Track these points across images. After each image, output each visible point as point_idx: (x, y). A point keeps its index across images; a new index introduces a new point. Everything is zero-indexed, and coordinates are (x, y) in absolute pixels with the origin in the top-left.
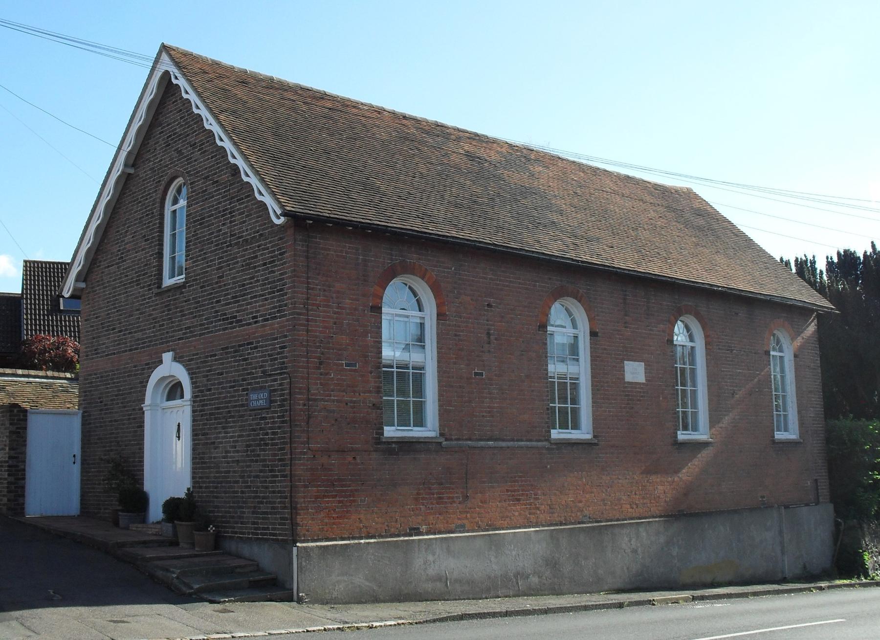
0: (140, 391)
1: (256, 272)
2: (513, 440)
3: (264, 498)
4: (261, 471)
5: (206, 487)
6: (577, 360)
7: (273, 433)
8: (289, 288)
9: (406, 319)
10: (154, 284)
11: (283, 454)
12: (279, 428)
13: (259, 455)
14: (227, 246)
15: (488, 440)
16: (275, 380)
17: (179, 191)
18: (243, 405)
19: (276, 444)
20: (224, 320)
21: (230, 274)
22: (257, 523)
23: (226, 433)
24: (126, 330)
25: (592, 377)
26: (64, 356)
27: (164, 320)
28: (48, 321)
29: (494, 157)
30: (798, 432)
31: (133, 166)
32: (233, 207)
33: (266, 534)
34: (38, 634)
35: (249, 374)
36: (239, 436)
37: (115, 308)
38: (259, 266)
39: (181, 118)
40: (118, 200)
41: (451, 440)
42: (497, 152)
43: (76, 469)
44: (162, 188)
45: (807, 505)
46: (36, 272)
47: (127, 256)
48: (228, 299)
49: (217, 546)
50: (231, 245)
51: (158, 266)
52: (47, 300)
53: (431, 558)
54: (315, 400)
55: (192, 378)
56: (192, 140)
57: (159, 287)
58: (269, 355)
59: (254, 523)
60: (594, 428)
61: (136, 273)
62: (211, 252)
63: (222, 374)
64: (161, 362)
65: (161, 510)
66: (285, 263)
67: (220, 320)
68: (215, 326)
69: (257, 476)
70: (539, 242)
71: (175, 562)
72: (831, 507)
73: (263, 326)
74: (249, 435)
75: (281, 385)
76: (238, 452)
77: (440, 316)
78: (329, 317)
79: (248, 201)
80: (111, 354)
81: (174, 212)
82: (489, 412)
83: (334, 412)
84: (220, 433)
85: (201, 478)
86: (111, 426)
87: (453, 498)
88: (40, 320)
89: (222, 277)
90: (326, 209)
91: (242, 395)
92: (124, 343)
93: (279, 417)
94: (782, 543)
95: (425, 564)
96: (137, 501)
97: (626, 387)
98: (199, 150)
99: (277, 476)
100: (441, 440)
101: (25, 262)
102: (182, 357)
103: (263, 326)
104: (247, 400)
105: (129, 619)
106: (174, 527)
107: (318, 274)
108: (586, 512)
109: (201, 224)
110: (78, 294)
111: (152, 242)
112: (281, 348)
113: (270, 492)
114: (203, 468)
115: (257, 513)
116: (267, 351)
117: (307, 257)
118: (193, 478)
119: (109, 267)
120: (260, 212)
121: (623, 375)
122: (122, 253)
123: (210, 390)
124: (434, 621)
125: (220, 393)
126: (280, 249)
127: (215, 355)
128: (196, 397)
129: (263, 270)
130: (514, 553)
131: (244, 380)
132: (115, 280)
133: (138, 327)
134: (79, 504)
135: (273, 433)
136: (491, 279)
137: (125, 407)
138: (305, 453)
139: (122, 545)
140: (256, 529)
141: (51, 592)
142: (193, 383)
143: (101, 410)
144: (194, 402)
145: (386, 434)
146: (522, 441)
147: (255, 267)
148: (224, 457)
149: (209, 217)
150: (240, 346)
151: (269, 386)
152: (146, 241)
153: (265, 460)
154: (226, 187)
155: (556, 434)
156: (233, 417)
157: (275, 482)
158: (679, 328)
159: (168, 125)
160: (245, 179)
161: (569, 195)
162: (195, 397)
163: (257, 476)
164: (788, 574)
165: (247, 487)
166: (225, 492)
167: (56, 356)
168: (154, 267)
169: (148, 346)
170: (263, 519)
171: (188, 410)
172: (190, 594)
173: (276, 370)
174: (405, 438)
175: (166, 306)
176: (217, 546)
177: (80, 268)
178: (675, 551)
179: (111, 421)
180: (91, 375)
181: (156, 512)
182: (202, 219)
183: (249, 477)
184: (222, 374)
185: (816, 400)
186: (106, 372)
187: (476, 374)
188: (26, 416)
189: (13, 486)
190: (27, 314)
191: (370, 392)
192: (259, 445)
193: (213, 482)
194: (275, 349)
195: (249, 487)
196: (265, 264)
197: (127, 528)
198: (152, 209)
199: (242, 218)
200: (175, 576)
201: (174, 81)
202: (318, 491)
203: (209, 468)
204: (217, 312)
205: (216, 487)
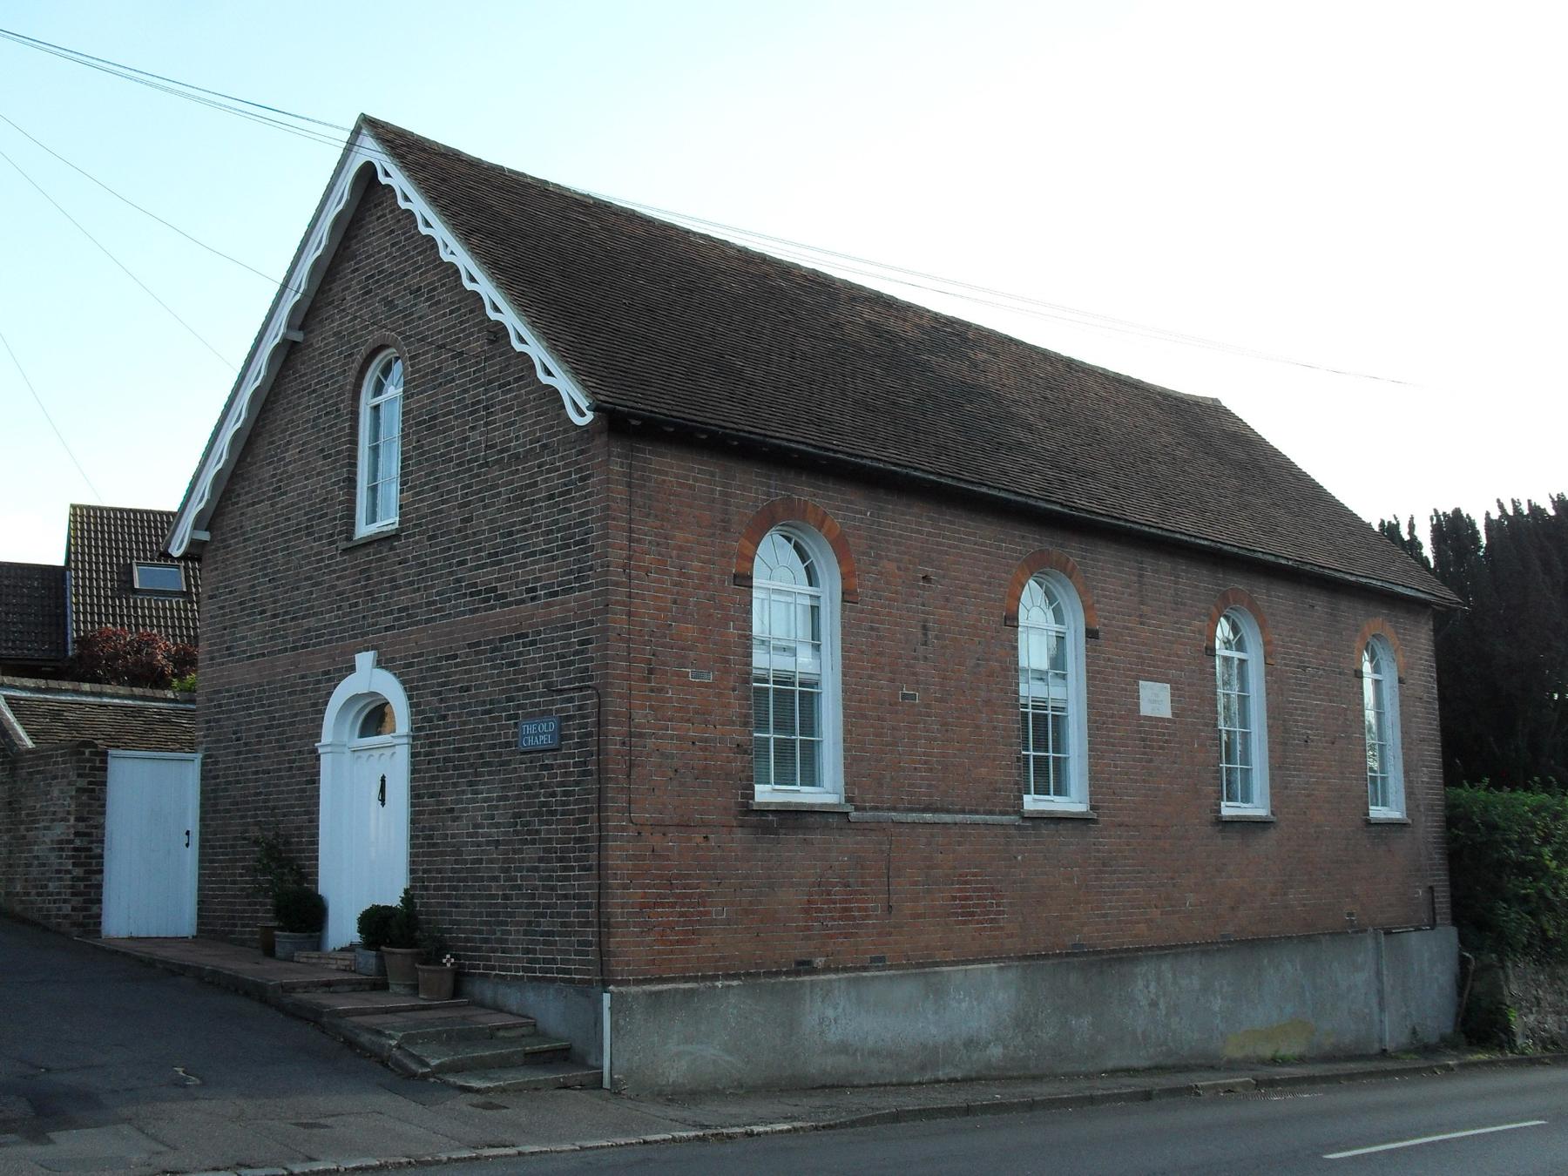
0: (313, 720)
1: (534, 511)
2: (963, 812)
3: (547, 906)
4: (541, 860)
5: (437, 888)
6: (1064, 677)
7: (565, 794)
8: (598, 538)
9: (789, 599)
10: (341, 533)
11: (584, 830)
12: (577, 783)
13: (538, 832)
14: (481, 466)
15: (925, 810)
16: (571, 700)
17: (386, 371)
18: (508, 744)
19: (572, 812)
20: (472, 594)
21: (484, 516)
22: (534, 951)
23: (476, 792)
24: (286, 613)
25: (1089, 706)
26: (150, 664)
27: (357, 596)
28: (114, 608)
29: (912, 333)
30: (1404, 807)
31: (301, 328)
32: (492, 398)
33: (550, 971)
34: (176, 1149)
35: (519, 689)
36: (500, 799)
37: (266, 575)
38: (540, 500)
39: (393, 245)
40: (272, 388)
41: (864, 809)
42: (917, 326)
43: (191, 856)
44: (356, 366)
45: (1418, 929)
46: (92, 526)
47: (288, 485)
48: (480, 558)
49: (457, 992)
50: (486, 464)
51: (348, 501)
52: (112, 572)
53: (830, 1013)
54: (641, 735)
55: (410, 698)
56: (413, 281)
57: (349, 539)
58: (559, 656)
59: (527, 951)
60: (1091, 793)
61: (306, 514)
62: (449, 476)
63: (468, 689)
64: (352, 669)
65: (355, 926)
66: (590, 494)
67: (465, 595)
68: (455, 607)
69: (536, 869)
70: (1006, 474)
71: (389, 1018)
72: (1453, 931)
73: (548, 605)
74: (518, 797)
75: (580, 708)
76: (497, 825)
77: (848, 596)
78: (665, 591)
79: (520, 388)
80: (258, 656)
81: (376, 408)
82: (926, 763)
83: (672, 756)
84: (463, 792)
85: (425, 871)
86: (256, 780)
87: (866, 909)
88: (99, 606)
89: (469, 519)
90: (662, 405)
91: (508, 727)
92: (283, 637)
93: (575, 765)
94: (1380, 992)
95: (821, 1024)
96: (307, 913)
97: (1142, 725)
98: (427, 300)
99: (572, 869)
100: (849, 808)
101: (74, 507)
102: (393, 660)
103: (548, 605)
104: (515, 735)
105: (329, 1121)
106: (380, 958)
107: (648, 515)
109: (429, 428)
110: (194, 551)
111: (336, 461)
112: (582, 643)
113: (559, 897)
114: (430, 854)
115: (535, 933)
116: (554, 648)
117: (629, 485)
118: (412, 871)
119: (253, 504)
120: (542, 405)
121: (1138, 705)
122: (280, 481)
123: (444, 717)
124: (853, 1124)
125: (465, 723)
126: (581, 470)
127: (456, 657)
128: (419, 729)
129: (548, 507)
130: (964, 1005)
131: (509, 700)
132: (266, 527)
133: (308, 609)
134: (195, 921)
135: (565, 794)
136: (929, 534)
137: (283, 748)
138: (623, 829)
139: (290, 988)
140: (530, 961)
141: (180, 1070)
142: (411, 706)
143: (238, 753)
144: (414, 738)
145: (759, 798)
146: (977, 812)
147: (532, 502)
148: (469, 835)
149: (445, 415)
150: (502, 640)
151: (557, 711)
152: (325, 458)
153: (550, 841)
154: (477, 363)
155: (1031, 803)
156: (489, 764)
157: (567, 878)
158: (1223, 630)
159: (368, 258)
160: (518, 347)
161: (1035, 401)
162: (416, 731)
163: (536, 869)
164: (1390, 1046)
165: (513, 888)
166: (473, 897)
167: (135, 664)
168: (340, 503)
169: (326, 642)
170: (545, 943)
171: (403, 755)
172: (425, 1076)
173: (570, 681)
174: (788, 804)
175: (361, 572)
176: (457, 992)
177: (202, 506)
179: (257, 773)
180: (219, 692)
181: (343, 929)
182: (431, 419)
183: (519, 869)
184: (468, 689)
185: (1432, 753)
186: (248, 687)
187: (904, 696)
188: (105, 762)
189: (82, 884)
190: (76, 595)
191: (733, 723)
192: (537, 814)
193: (450, 879)
194: (569, 645)
195: (519, 887)
196: (551, 497)
197: (290, 959)
198: (336, 404)
199: (509, 417)
200: (394, 1043)
201: (383, 180)
202: (645, 896)
203: (442, 854)
204: (458, 581)
205: (456, 888)
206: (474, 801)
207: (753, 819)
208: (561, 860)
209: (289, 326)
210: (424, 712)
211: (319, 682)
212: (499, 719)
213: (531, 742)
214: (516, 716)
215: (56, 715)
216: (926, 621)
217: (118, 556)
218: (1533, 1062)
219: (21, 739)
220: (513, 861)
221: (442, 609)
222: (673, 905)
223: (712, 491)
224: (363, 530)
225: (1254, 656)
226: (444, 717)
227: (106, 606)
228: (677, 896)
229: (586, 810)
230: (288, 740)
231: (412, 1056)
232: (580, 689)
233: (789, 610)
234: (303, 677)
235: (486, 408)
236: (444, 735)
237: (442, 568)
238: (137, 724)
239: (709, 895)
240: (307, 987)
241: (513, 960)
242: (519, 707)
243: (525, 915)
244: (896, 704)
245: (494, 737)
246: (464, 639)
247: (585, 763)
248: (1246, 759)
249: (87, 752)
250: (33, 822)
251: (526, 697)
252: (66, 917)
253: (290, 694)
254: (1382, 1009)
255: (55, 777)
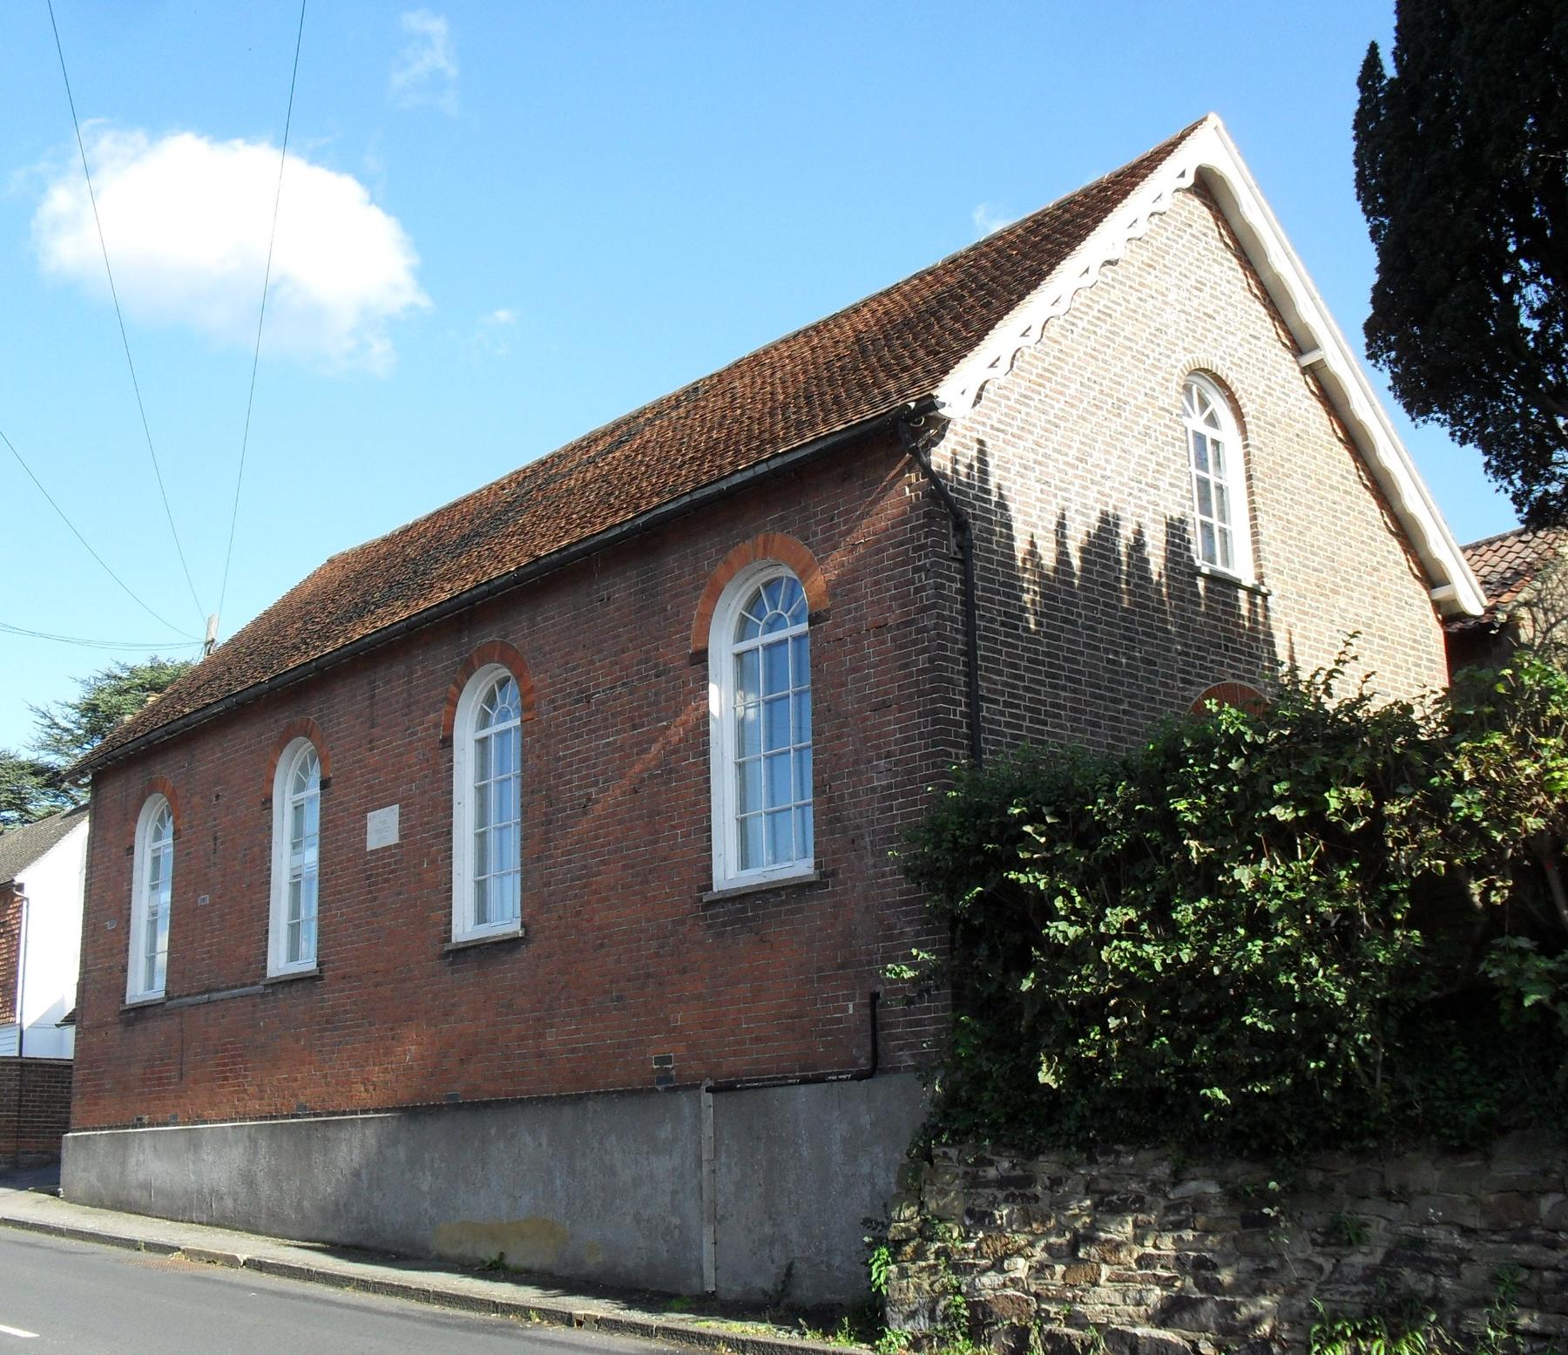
108: (302, 1099)
178: (426, 1182)
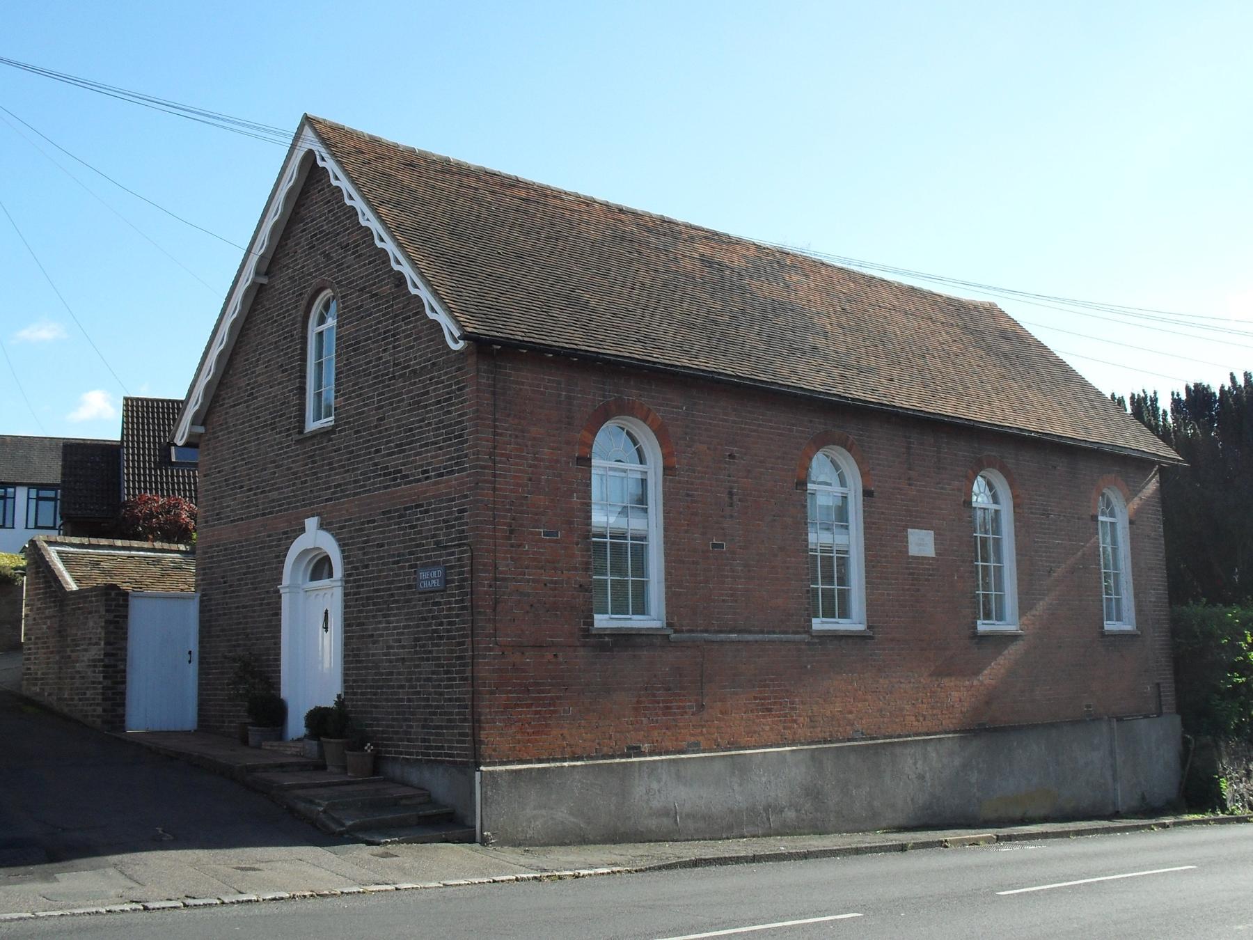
0: (276, 568)
1: (427, 413)
2: (762, 632)
3: (437, 707)
4: (433, 673)
5: (362, 694)
6: (847, 528)
7: (450, 623)
9: (623, 474)
12: (457, 616)
13: (430, 652)
14: (390, 379)
15: (731, 632)
16: (452, 554)
17: (327, 307)
18: (410, 587)
19: (454, 637)
20: (385, 475)
21: (393, 416)
22: (429, 741)
23: (388, 622)
24: (258, 488)
27: (307, 475)
28: (156, 476)
29: (738, 263)
31: (267, 274)
35: (417, 546)
36: (405, 627)
38: (431, 405)
40: (247, 319)
41: (682, 631)
42: (742, 256)
43: (193, 670)
44: (304, 302)
45: (1146, 717)
46: (142, 414)
49: (376, 770)
50: (394, 378)
53: (655, 786)
54: (504, 580)
55: (343, 552)
56: (342, 239)
58: (445, 521)
60: (868, 616)
64: (303, 530)
65: (303, 723)
66: (465, 401)
67: (380, 475)
68: (374, 484)
69: (429, 679)
70: (796, 373)
71: (322, 791)
75: (459, 559)
76: (403, 647)
77: (668, 470)
79: (416, 321)
81: (320, 334)
83: (528, 595)
84: (380, 622)
85: (354, 681)
86: (238, 613)
89: (382, 419)
90: (518, 331)
91: (410, 574)
95: (647, 793)
96: (272, 712)
99: (455, 679)
101: (126, 399)
104: (415, 579)
105: (262, 866)
106: (320, 746)
107: (509, 415)
109: (355, 350)
110: (193, 440)
112: (460, 511)
113: (445, 700)
114: (357, 668)
115: (429, 727)
117: (494, 393)
118: (345, 681)
121: (907, 547)
123: (367, 566)
124: (660, 868)
125: (381, 571)
127: (374, 521)
129: (437, 410)
131: (411, 553)
132: (243, 423)
135: (450, 623)
136: (734, 422)
138: (491, 649)
139: (252, 769)
140: (427, 748)
141: (160, 830)
142: (344, 558)
143: (225, 593)
144: (346, 582)
145: (597, 624)
146: (774, 633)
149: (366, 340)
150: (406, 509)
151: (445, 562)
152: (283, 372)
153: (438, 658)
155: (818, 624)
156: (397, 602)
157: (451, 686)
158: (979, 485)
161: (835, 312)
162: (347, 576)
166: (387, 700)
167: (165, 522)
169: (285, 510)
170: (437, 734)
171: (338, 593)
172: (341, 834)
173: (453, 540)
175: (310, 457)
176: (376, 770)
179: (237, 607)
180: (211, 547)
181: (296, 726)
183: (418, 680)
184: (382, 545)
187: (714, 546)
188: (127, 600)
190: (128, 468)
191: (576, 569)
192: (431, 638)
193: (371, 687)
195: (419, 693)
196: (439, 402)
200: (321, 809)
201: (321, 164)
202: (508, 699)
203: (366, 668)
204: (376, 464)
205: (375, 694)
206: (387, 628)
207: (592, 640)
208: (447, 672)
209: (257, 273)
210: (351, 562)
211: (280, 540)
212: (403, 567)
213: (425, 585)
214: (416, 566)
215: (95, 565)
216: (731, 488)
217: (159, 437)
218: (1240, 820)
219: (67, 583)
220: (414, 673)
221: (364, 486)
222: (530, 706)
223: (560, 395)
224: (312, 425)
225: (1006, 508)
226: (367, 566)
227: (150, 476)
228: (534, 699)
229: (463, 636)
230: (259, 583)
231: (333, 819)
232: (459, 546)
233: (622, 484)
234: (269, 536)
235: (393, 335)
236: (367, 579)
237: (365, 455)
238: (156, 570)
239: (558, 698)
240: (266, 768)
241: (414, 747)
242: (418, 559)
243: (422, 713)
244: (708, 551)
245: (400, 581)
246: (380, 508)
247: (462, 601)
248: (999, 586)
249: (113, 593)
250: (77, 645)
251: (422, 551)
252: (98, 716)
253: (260, 548)
254: (1115, 780)
255: (90, 613)
